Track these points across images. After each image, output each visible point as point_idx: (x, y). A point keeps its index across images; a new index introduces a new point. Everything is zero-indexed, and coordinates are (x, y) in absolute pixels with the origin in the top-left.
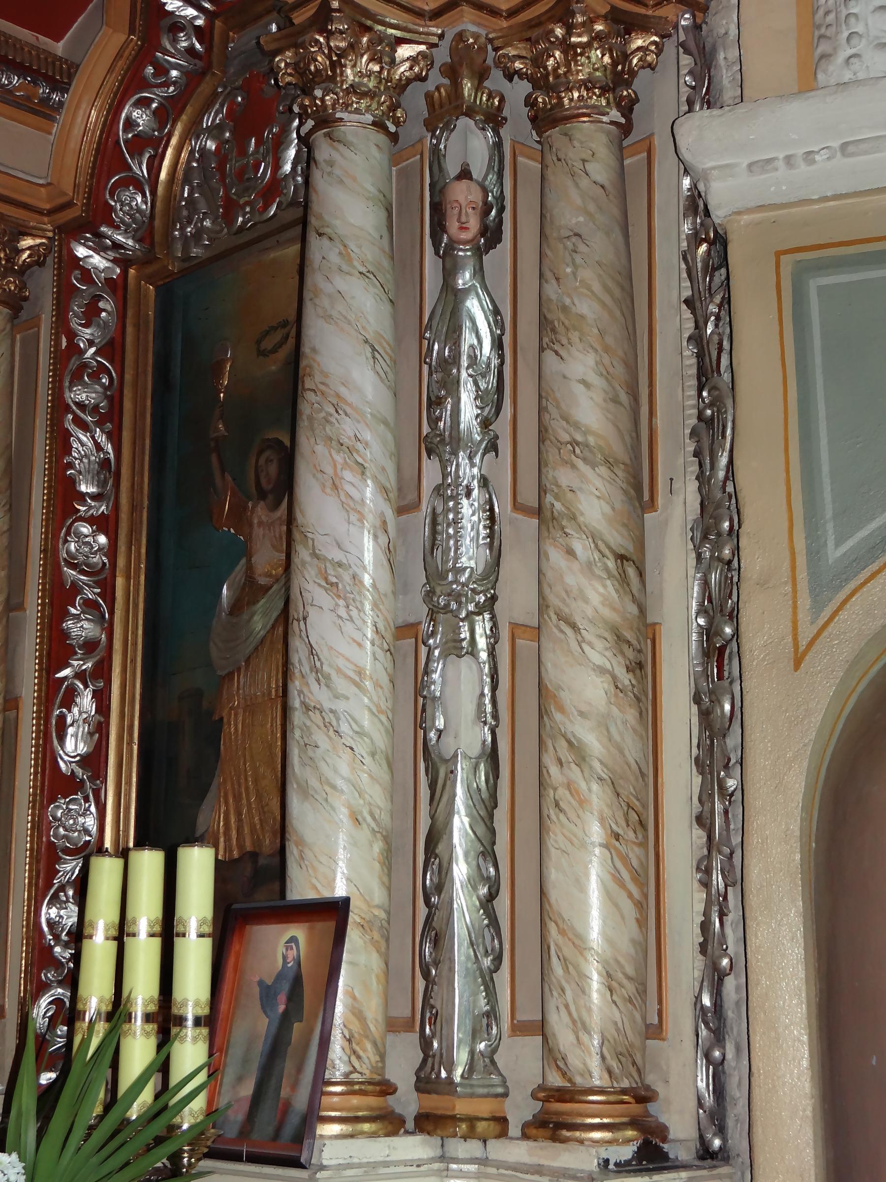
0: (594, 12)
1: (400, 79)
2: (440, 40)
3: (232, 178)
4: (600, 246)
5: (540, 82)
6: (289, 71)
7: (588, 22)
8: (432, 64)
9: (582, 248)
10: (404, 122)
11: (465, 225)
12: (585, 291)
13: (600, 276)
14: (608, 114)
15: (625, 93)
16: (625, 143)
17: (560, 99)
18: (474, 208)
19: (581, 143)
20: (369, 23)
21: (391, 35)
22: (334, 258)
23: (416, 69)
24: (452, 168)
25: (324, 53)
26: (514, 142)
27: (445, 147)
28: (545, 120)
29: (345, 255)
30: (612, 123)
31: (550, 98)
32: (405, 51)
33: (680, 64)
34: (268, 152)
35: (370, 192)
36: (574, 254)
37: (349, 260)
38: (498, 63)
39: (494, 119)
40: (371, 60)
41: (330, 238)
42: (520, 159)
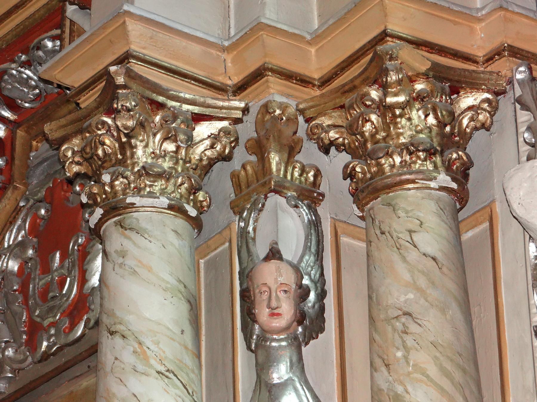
0: (412, 69)
1: (201, 160)
2: (244, 114)
3: (35, 299)
4: (436, 325)
5: (358, 152)
6: (77, 159)
7: (406, 80)
8: (237, 140)
9: (413, 328)
10: (209, 206)
11: (278, 313)
12: (418, 376)
13: (436, 358)
14: (435, 178)
15: (455, 156)
16: (462, 215)
17: (379, 165)
18: (285, 291)
19: (407, 212)
20: (161, 99)
21: (188, 111)
22: (128, 357)
23: (219, 147)
24: (261, 250)
25: (113, 136)
26: (335, 221)
27: (254, 230)
28: (367, 191)
29: (141, 353)
30: (442, 189)
31: (369, 165)
32: (203, 130)
33: (519, 121)
34: (73, 266)
35: (168, 282)
36: (404, 335)
37: (145, 359)
38: (311, 135)
39: (310, 196)
40: (166, 139)
41: (124, 337)
42: (344, 240)
